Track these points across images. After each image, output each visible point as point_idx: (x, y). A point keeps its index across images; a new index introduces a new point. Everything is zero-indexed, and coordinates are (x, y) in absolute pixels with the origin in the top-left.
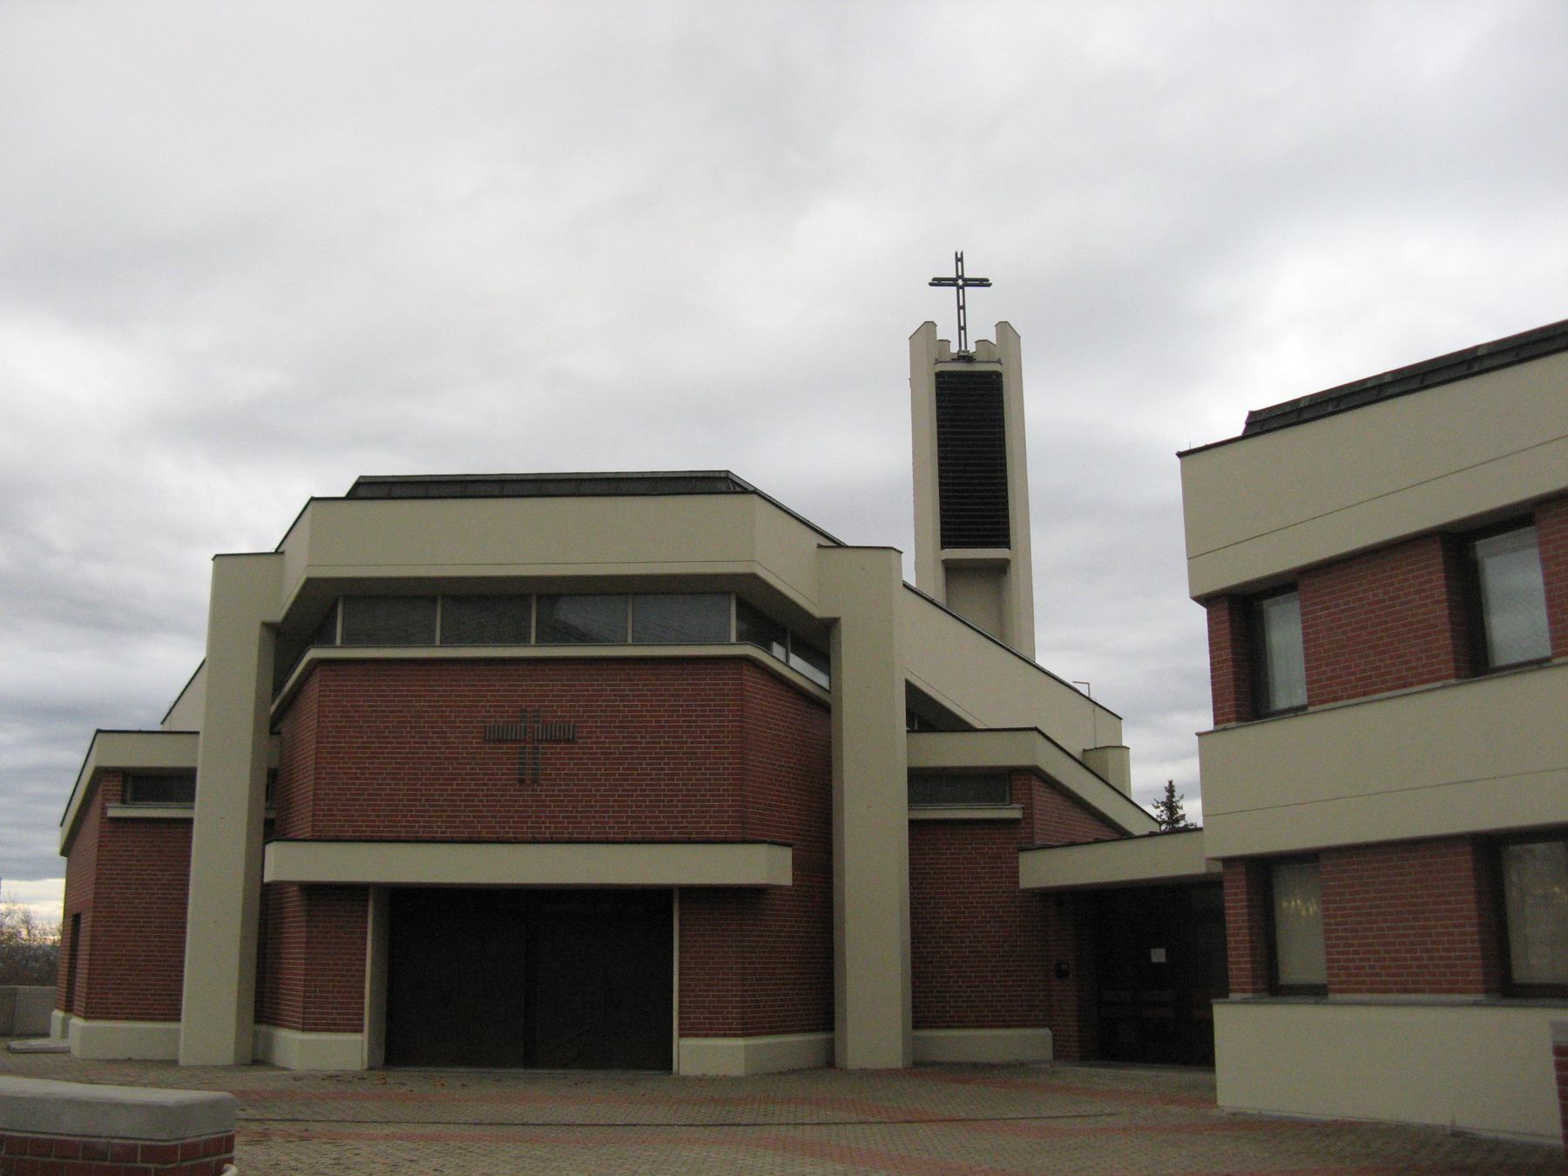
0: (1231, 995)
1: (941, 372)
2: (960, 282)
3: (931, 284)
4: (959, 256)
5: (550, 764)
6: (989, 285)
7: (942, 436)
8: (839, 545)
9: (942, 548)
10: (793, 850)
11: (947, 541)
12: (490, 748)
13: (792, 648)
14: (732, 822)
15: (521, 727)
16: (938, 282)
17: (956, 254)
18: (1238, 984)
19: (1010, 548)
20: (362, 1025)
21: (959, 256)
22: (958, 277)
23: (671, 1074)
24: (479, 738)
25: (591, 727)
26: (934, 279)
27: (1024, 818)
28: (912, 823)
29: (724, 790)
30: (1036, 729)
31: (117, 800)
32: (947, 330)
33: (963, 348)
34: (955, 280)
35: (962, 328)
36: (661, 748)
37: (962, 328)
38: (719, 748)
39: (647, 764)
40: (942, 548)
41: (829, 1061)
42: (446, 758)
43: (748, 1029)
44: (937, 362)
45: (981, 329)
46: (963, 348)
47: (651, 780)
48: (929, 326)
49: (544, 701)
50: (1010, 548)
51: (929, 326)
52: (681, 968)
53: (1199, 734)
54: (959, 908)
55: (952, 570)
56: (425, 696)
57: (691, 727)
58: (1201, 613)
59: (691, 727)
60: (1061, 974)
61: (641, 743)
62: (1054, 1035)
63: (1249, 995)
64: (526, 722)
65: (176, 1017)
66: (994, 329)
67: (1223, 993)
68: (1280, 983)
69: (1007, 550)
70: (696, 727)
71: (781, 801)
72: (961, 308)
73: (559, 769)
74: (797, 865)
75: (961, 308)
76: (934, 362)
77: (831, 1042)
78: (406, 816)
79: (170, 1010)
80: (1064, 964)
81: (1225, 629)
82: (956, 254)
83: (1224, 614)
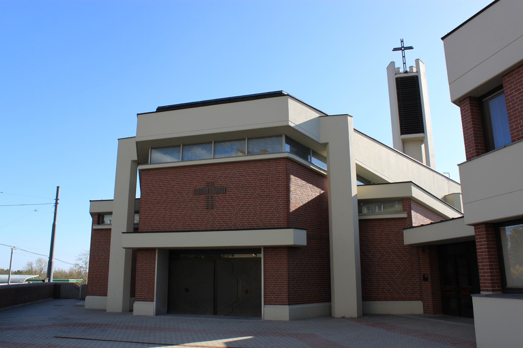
0: (482, 292)
1: (397, 77)
2: (403, 49)
3: (393, 50)
4: (402, 40)
5: (217, 202)
6: (413, 48)
7: (399, 98)
8: (327, 115)
9: (401, 135)
10: (307, 231)
11: (402, 133)
12: (197, 197)
13: (312, 155)
14: (284, 221)
15: (207, 189)
16: (395, 49)
17: (401, 39)
18: (485, 287)
19: (424, 133)
20: (154, 299)
21: (402, 40)
22: (402, 47)
23: (261, 319)
24: (193, 194)
25: (232, 188)
26: (394, 49)
27: (408, 217)
28: (360, 221)
29: (280, 209)
30: (411, 182)
31: (96, 223)
32: (399, 64)
33: (405, 70)
34: (402, 48)
35: (404, 63)
36: (257, 194)
37: (404, 63)
38: (278, 193)
39: (252, 200)
40: (401, 135)
41: (329, 314)
42: (182, 202)
43: (291, 302)
44: (396, 74)
45: (410, 62)
46: (405, 70)
47: (253, 206)
48: (392, 63)
49: (215, 179)
50: (424, 133)
51: (392, 63)
52: (264, 278)
53: (458, 165)
54: (383, 253)
55: (404, 142)
56: (175, 180)
57: (268, 185)
58: (457, 109)
59: (268, 185)
60: (425, 279)
61: (249, 192)
62: (423, 304)
63: (491, 293)
64: (209, 187)
65: (106, 296)
66: (415, 61)
67: (477, 291)
68: (508, 287)
69: (423, 134)
70: (270, 185)
71: (307, 213)
72: (404, 57)
73: (220, 204)
74: (309, 238)
75: (404, 57)
76: (394, 74)
77: (330, 307)
78: (169, 223)
79: (104, 293)
80: (426, 275)
81: (468, 114)
82: (401, 39)
83: (468, 107)
